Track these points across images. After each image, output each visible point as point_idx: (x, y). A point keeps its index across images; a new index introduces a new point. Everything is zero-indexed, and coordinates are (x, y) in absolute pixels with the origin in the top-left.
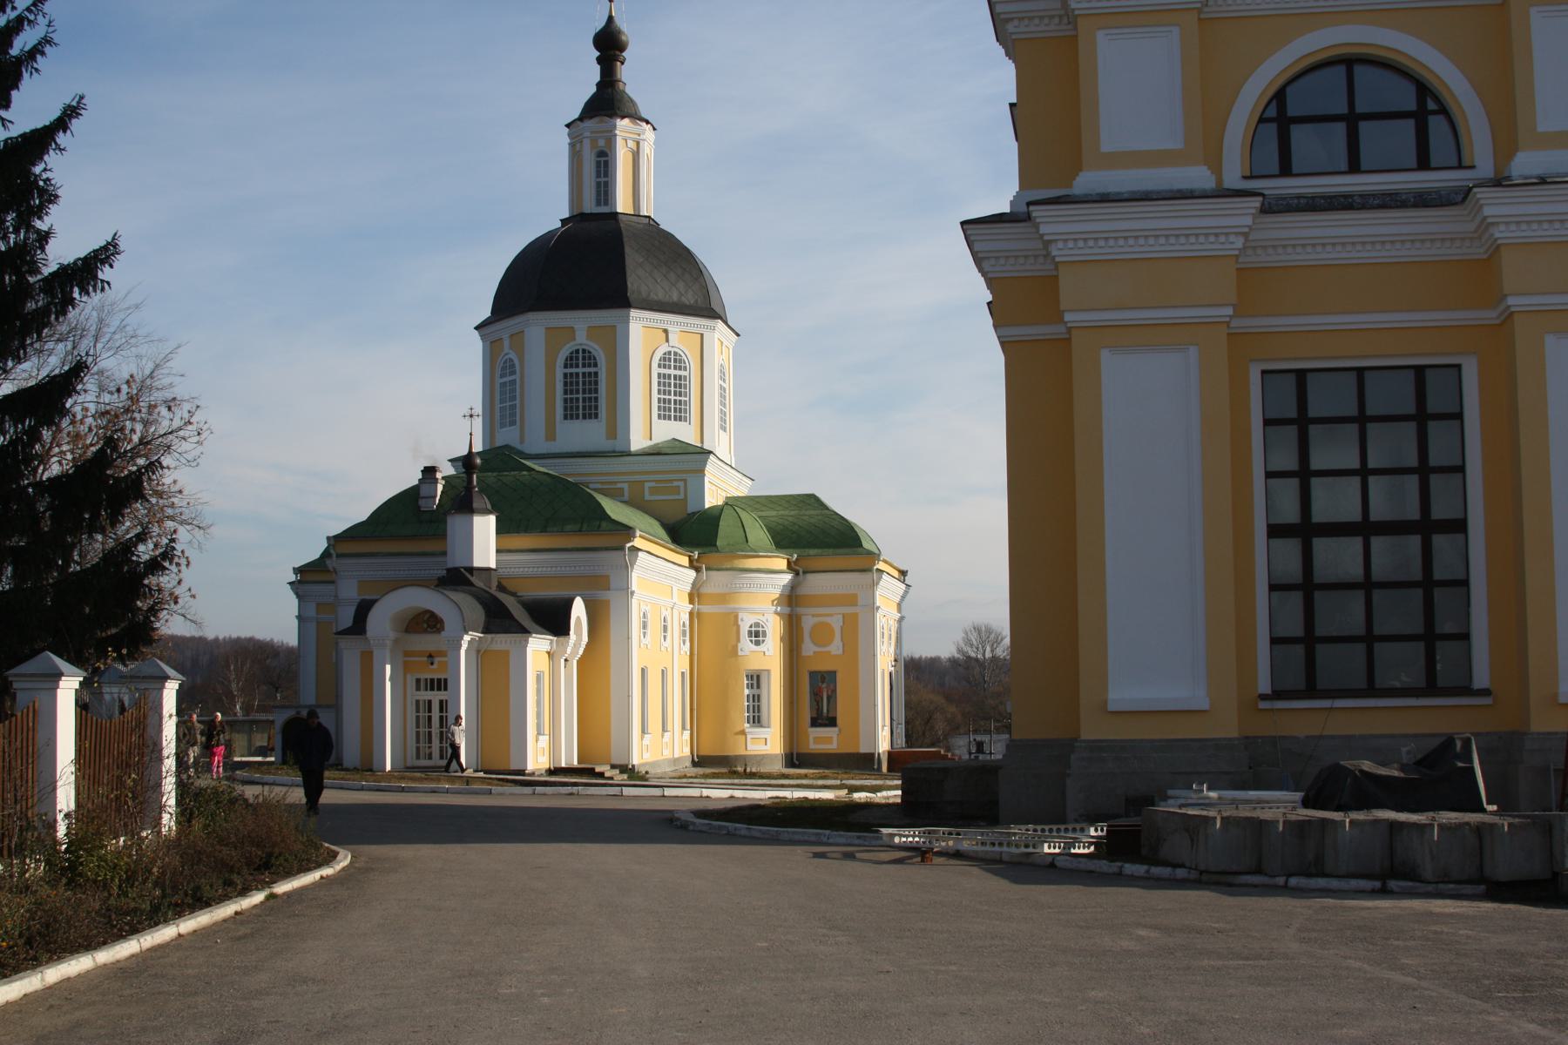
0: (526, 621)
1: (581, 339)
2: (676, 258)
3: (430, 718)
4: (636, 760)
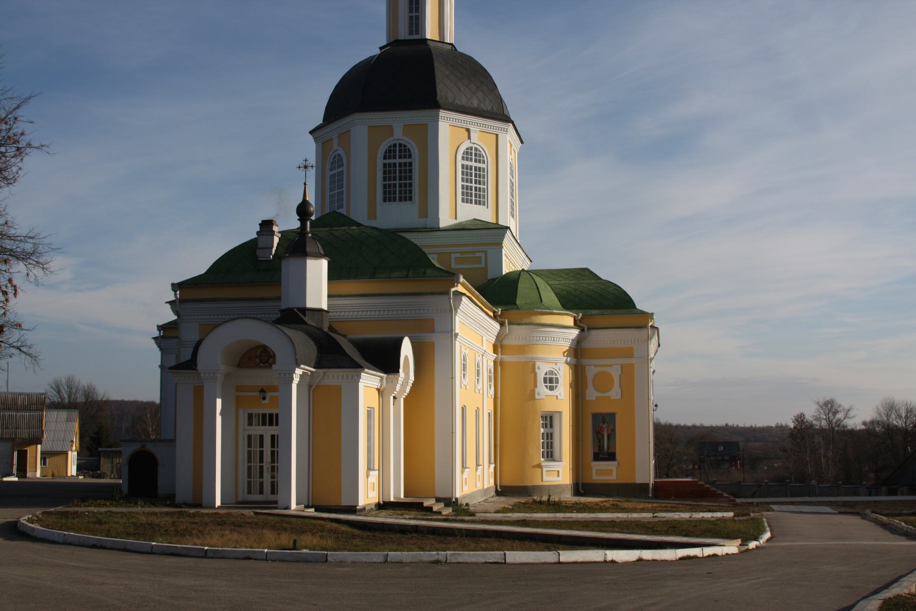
1: (399, 135)
2: (475, 75)
3: (262, 453)
4: (458, 494)
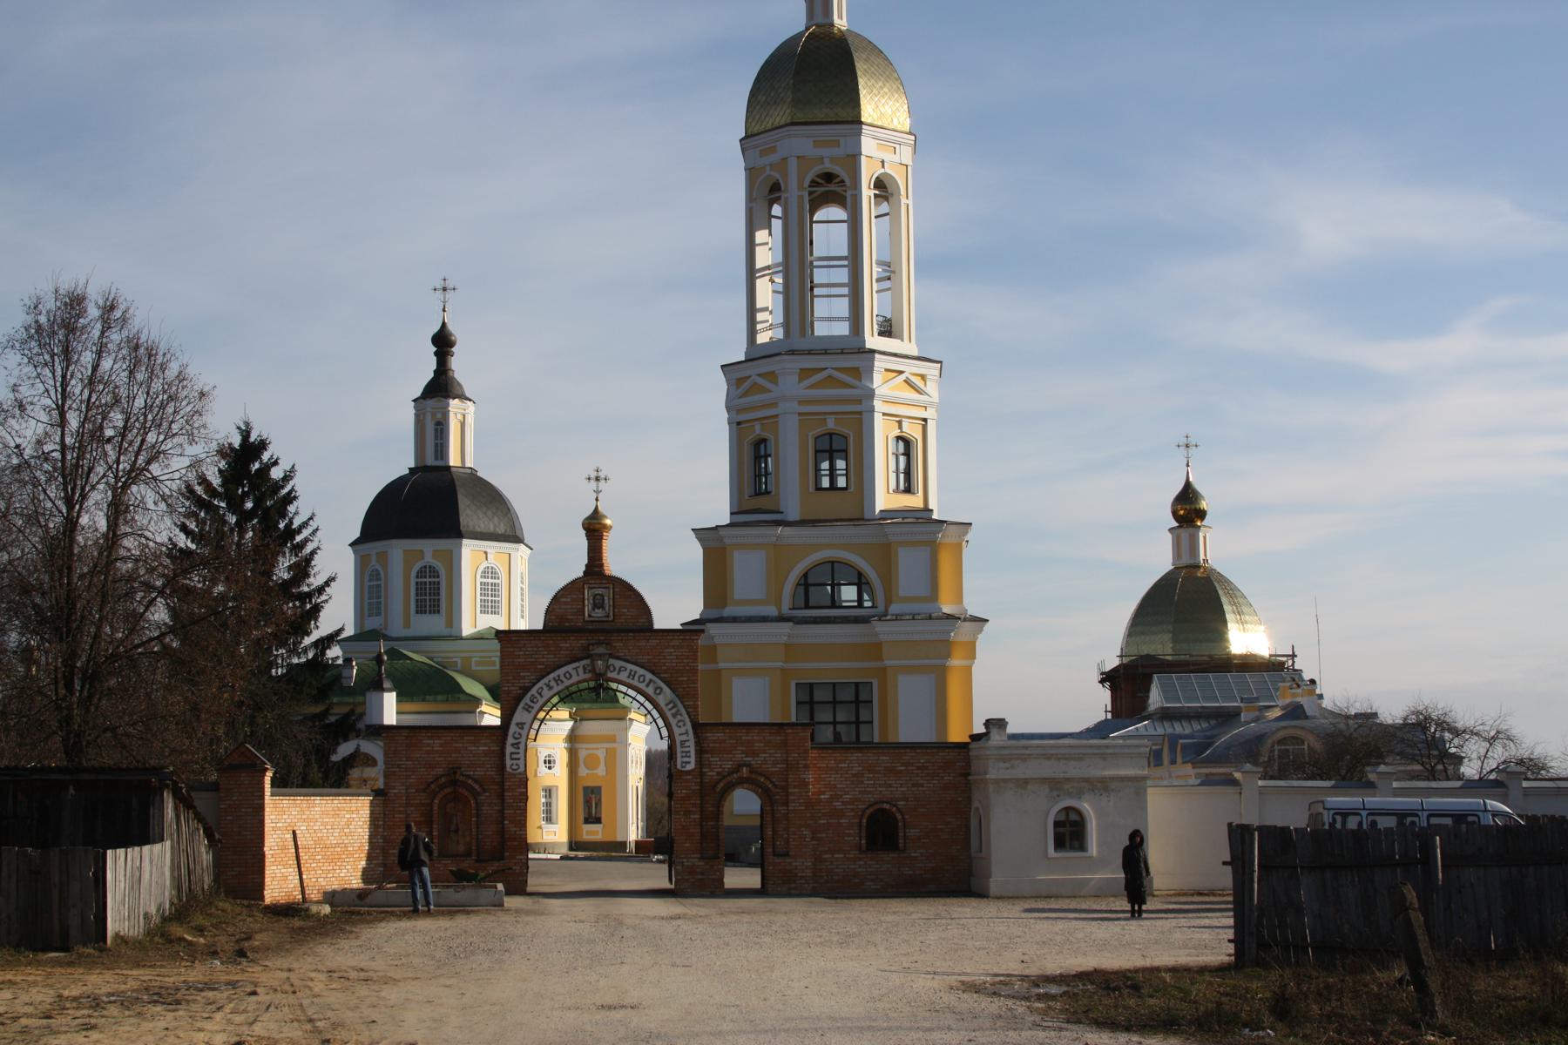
1: (429, 559)
2: (492, 498)
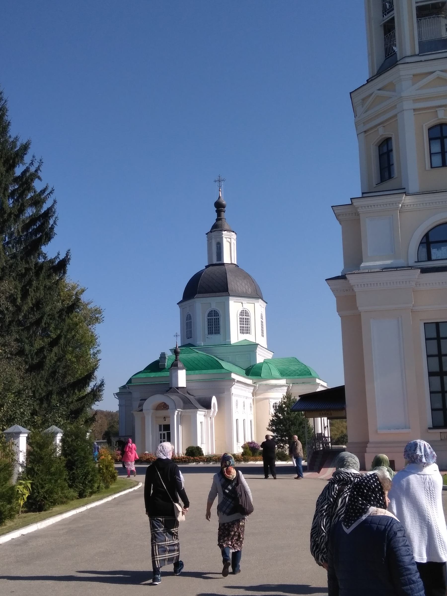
0: (198, 405)
